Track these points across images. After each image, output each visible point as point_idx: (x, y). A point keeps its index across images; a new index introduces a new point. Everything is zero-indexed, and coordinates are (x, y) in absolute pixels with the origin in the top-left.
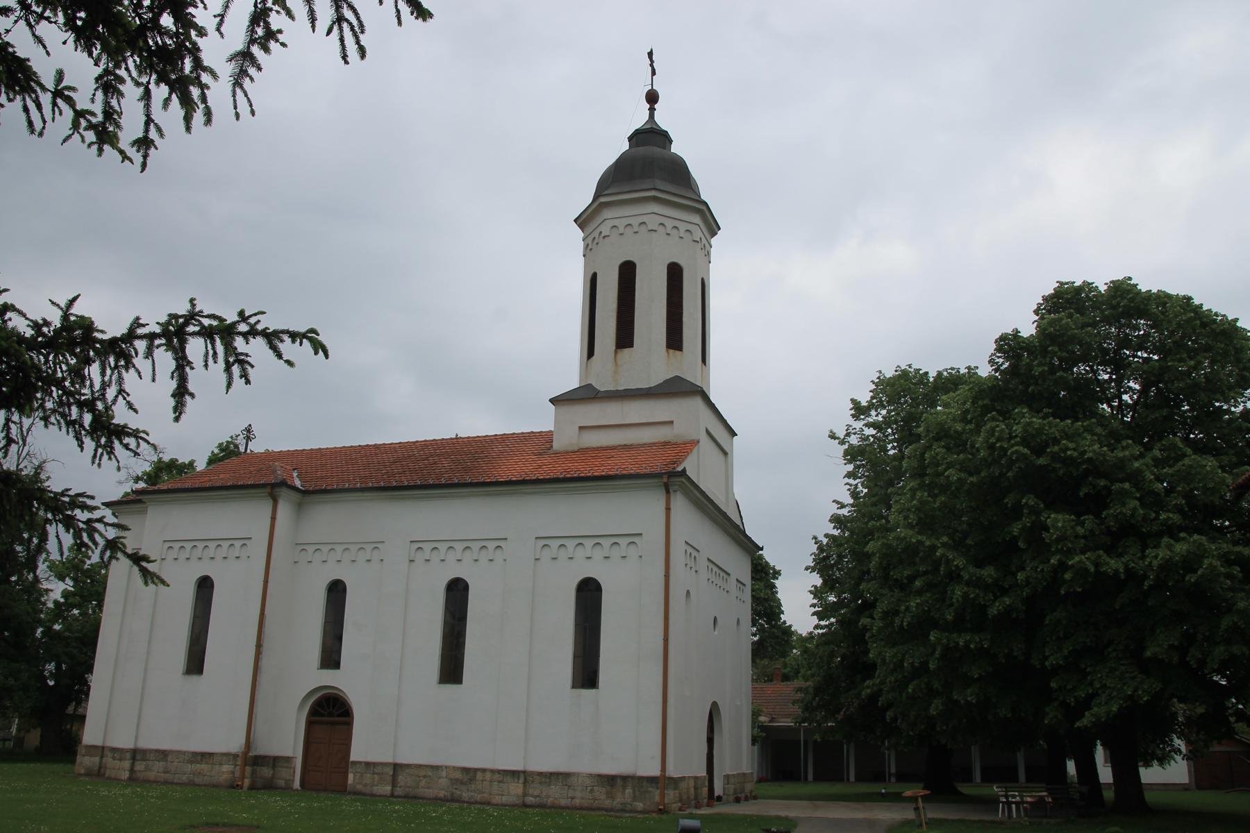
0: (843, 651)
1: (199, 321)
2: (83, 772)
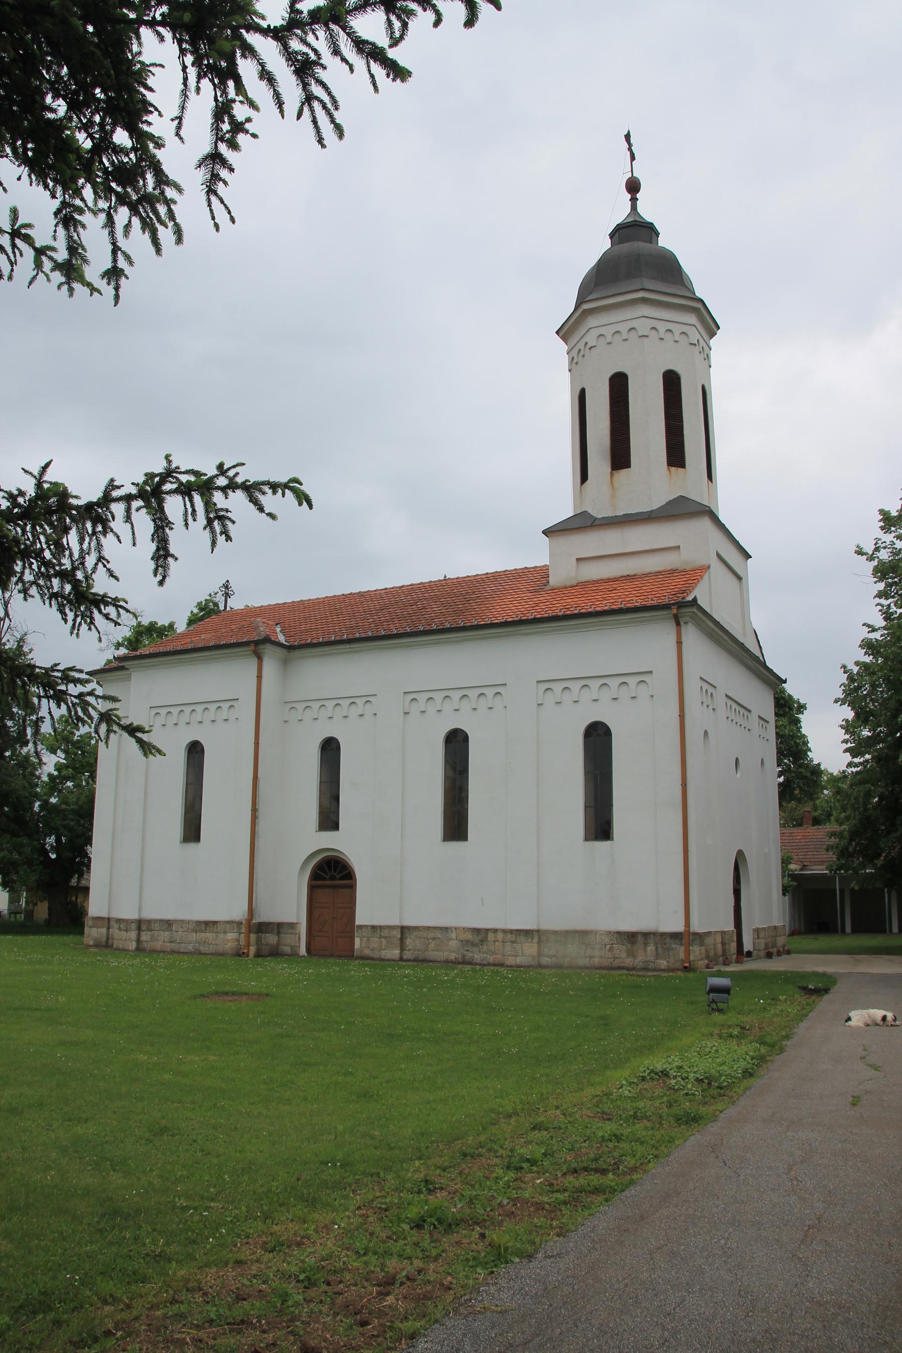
0: (881, 790)
1: (176, 478)
2: (91, 943)
